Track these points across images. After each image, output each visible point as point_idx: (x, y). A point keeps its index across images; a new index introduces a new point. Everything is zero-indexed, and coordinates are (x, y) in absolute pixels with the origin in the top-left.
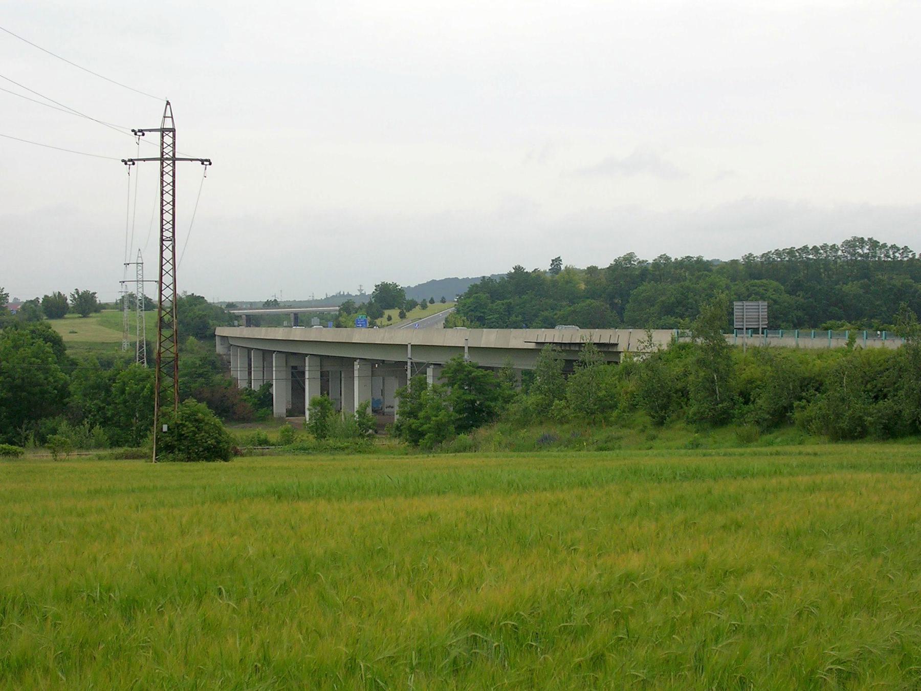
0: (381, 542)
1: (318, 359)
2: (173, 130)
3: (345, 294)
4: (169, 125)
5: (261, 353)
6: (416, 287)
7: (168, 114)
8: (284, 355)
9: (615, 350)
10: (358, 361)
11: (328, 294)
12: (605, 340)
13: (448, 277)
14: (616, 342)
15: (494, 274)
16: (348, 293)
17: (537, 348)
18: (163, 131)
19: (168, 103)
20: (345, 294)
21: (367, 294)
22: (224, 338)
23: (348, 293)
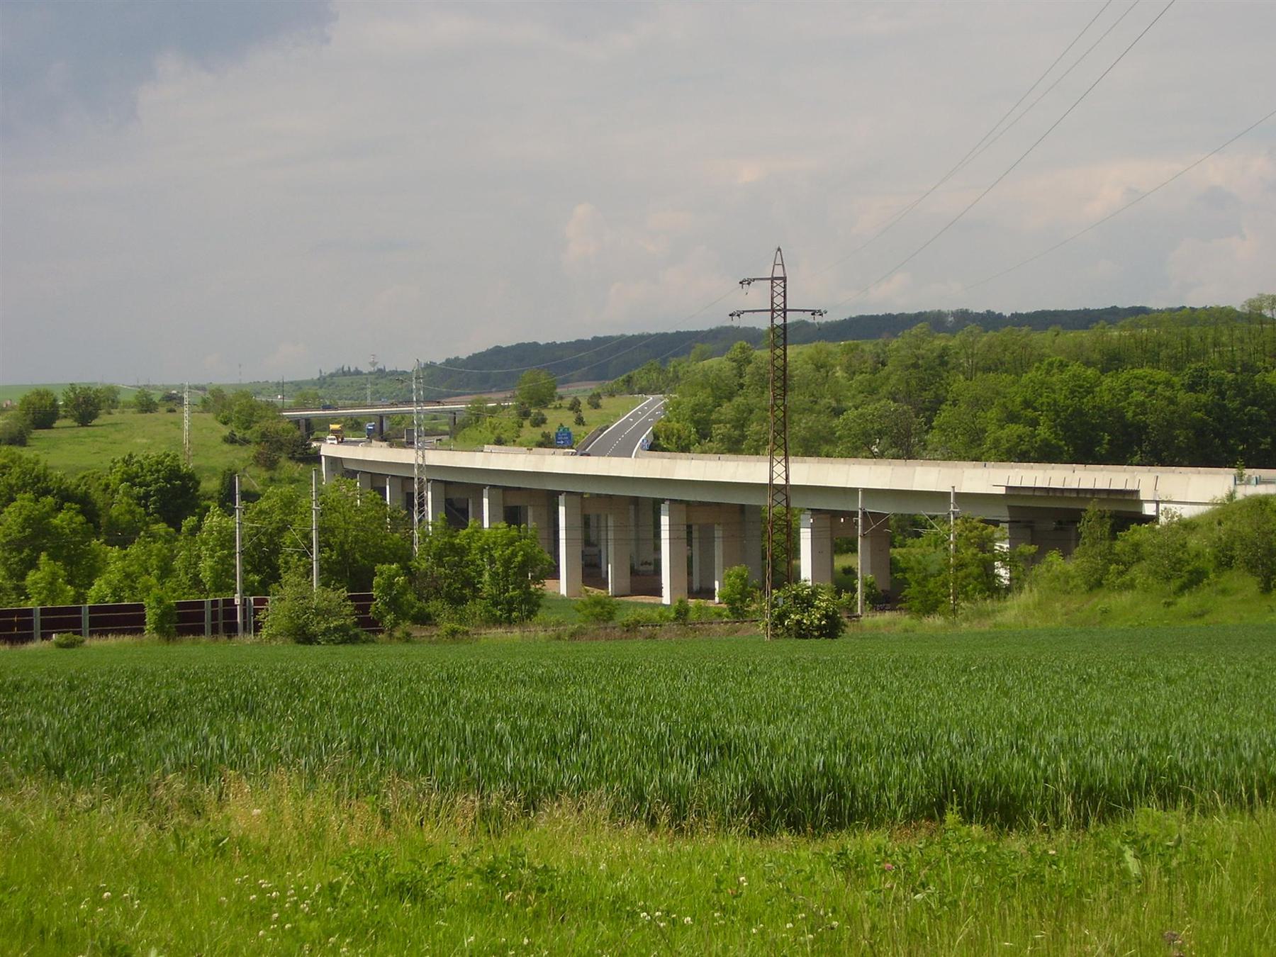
0: (129, 753)
1: (442, 487)
2: (784, 279)
3: (352, 370)
4: (779, 272)
5: (399, 481)
6: (469, 358)
7: (779, 261)
8: (683, 507)
9: (1135, 498)
10: (667, 503)
11: (323, 371)
12: (1118, 485)
13: (520, 342)
14: (1136, 488)
15: (598, 335)
16: (356, 368)
17: (1008, 493)
18: (773, 279)
19: (779, 249)
20: (352, 370)
21: (387, 370)
22: (334, 462)
23: (356, 368)
